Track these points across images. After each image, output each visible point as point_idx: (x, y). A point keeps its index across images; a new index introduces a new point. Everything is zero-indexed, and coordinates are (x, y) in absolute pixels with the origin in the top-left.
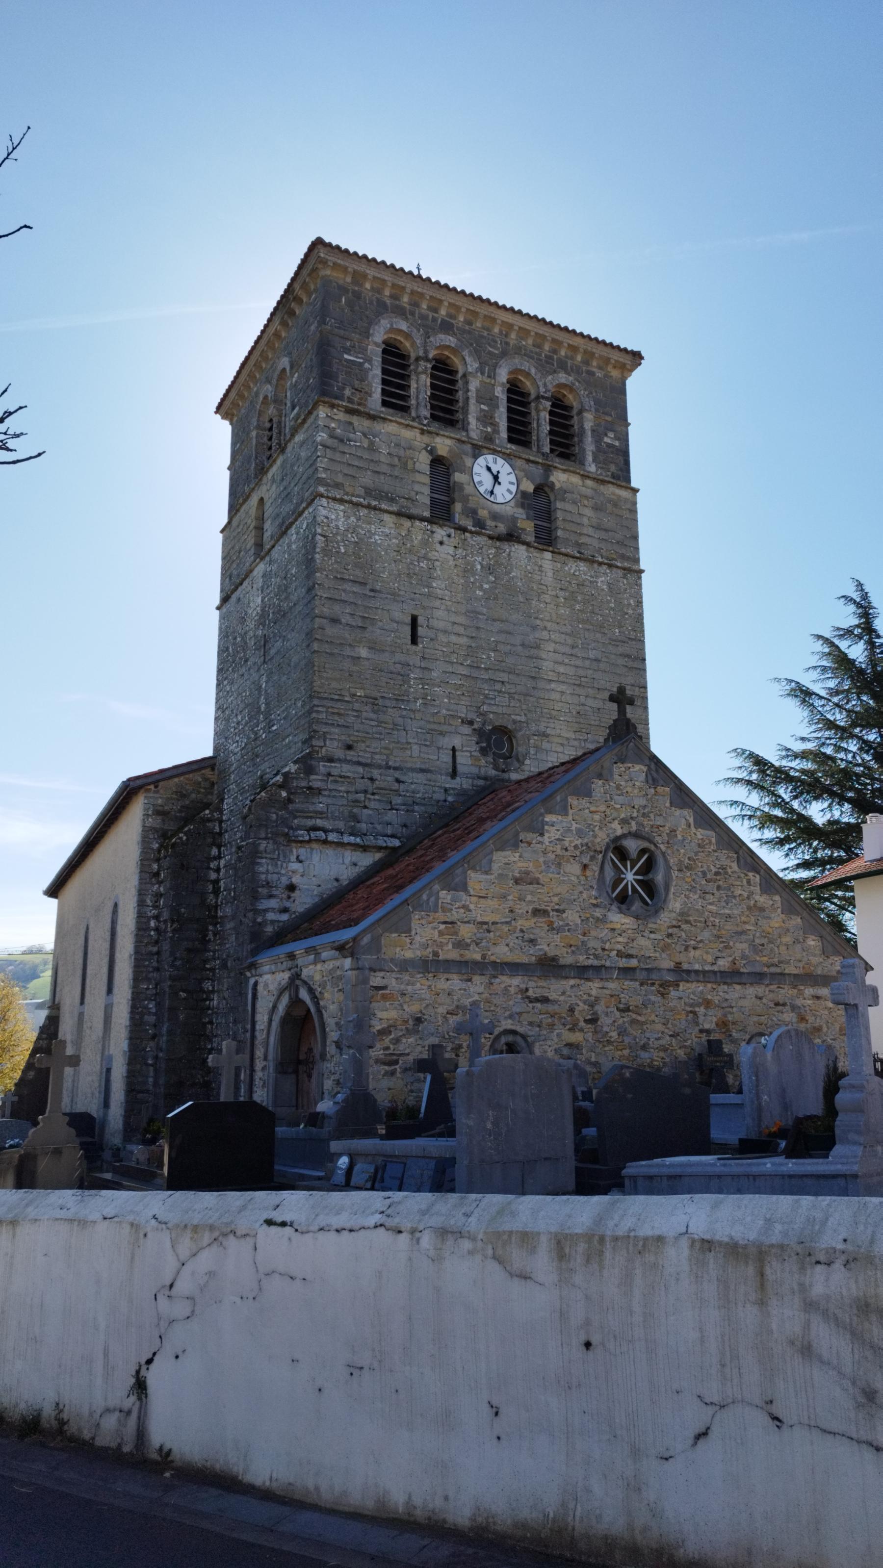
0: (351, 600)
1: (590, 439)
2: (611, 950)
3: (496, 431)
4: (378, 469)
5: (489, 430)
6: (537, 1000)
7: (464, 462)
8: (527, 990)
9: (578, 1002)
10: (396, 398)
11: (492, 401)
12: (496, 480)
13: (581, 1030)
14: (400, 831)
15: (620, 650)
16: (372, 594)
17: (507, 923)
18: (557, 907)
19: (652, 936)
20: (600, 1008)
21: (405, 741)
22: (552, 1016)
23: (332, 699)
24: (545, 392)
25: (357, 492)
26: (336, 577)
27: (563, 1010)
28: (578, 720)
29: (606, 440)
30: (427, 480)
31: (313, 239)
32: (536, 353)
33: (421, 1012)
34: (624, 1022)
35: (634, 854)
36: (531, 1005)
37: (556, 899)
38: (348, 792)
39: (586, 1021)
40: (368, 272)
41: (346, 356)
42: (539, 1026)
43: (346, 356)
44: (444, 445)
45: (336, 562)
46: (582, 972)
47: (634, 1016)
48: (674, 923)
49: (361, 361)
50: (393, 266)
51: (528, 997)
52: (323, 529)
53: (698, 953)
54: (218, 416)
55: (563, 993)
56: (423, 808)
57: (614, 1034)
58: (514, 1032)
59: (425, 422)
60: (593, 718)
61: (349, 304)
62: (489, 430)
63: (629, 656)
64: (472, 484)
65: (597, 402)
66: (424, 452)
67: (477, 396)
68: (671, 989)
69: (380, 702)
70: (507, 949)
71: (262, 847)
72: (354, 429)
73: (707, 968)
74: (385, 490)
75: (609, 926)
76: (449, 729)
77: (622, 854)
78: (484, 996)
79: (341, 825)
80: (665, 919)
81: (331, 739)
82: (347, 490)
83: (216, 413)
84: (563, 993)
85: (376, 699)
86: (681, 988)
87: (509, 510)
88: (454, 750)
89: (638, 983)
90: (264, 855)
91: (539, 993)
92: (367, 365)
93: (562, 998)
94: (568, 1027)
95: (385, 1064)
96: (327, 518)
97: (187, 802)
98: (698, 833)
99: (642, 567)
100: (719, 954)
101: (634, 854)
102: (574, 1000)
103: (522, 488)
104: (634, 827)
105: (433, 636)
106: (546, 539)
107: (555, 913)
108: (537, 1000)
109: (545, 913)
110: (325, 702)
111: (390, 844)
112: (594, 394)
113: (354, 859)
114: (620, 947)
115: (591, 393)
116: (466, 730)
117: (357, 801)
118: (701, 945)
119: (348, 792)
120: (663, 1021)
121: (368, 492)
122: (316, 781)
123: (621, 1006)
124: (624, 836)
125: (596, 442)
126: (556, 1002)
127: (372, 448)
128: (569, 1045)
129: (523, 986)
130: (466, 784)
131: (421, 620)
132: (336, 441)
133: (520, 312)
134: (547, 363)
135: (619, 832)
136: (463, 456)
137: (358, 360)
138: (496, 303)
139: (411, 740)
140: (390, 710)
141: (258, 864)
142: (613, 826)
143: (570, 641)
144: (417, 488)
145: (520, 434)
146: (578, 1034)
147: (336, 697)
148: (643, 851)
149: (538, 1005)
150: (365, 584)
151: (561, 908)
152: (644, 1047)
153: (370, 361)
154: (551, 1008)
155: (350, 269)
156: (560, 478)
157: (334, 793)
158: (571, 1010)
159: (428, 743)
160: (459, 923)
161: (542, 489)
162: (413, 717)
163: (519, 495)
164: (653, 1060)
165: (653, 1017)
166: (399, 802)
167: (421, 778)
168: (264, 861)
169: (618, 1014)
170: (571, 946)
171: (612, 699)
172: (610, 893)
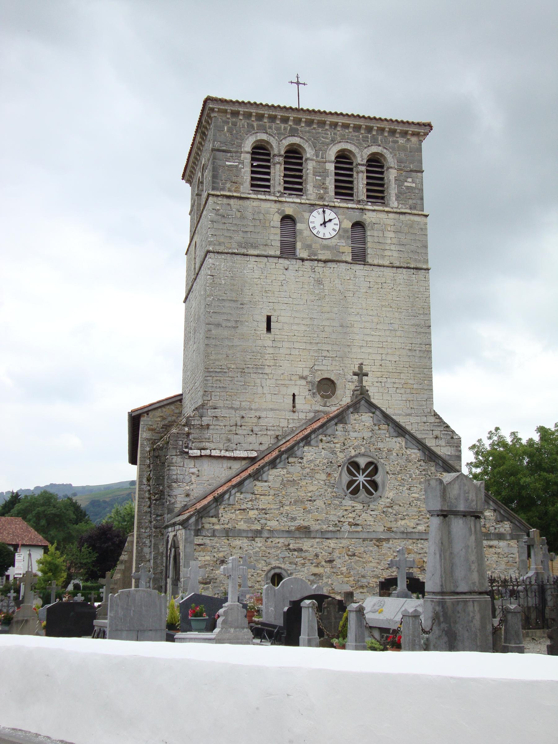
0: (229, 312)
1: (394, 186)
2: (344, 522)
3: (326, 193)
4: (246, 230)
5: (322, 192)
6: (295, 550)
7: (303, 215)
8: (289, 545)
9: (322, 551)
10: (260, 182)
11: (324, 173)
12: (324, 225)
13: (323, 566)
14: (257, 447)
15: (413, 322)
16: (242, 306)
17: (277, 508)
18: (310, 499)
19: (372, 513)
20: (336, 554)
21: (261, 392)
22: (304, 559)
23: (216, 372)
24: (362, 161)
25: (233, 246)
26: (219, 299)
27: (310, 556)
28: (380, 370)
29: (406, 184)
30: (278, 231)
31: (203, 99)
32: (356, 136)
33: (224, 557)
34: (351, 563)
35: (362, 466)
36: (291, 553)
37: (309, 494)
38: (225, 426)
39: (325, 562)
40: (240, 109)
41: (228, 163)
42: (296, 564)
43: (228, 163)
44: (291, 204)
45: (219, 290)
46: (324, 535)
47: (358, 559)
48: (388, 505)
49: (237, 164)
50: (255, 103)
51: (289, 549)
52: (211, 272)
53: (403, 522)
54: (184, 181)
55: (312, 546)
56: (273, 432)
57: (344, 569)
58: (280, 568)
59: (278, 195)
60: (391, 368)
61: (230, 130)
62: (322, 192)
63: (418, 325)
64: (308, 228)
65: (400, 161)
66: (276, 214)
67: (314, 172)
68: (384, 543)
69: (246, 370)
70: (277, 523)
71: (174, 461)
72: (231, 208)
73: (410, 530)
74: (251, 242)
75: (343, 508)
76: (290, 382)
77: (356, 465)
78: (262, 548)
79: (221, 446)
80: (383, 502)
81: (215, 395)
82: (227, 246)
83: (183, 179)
84: (312, 546)
85: (243, 369)
86: (391, 542)
87: (334, 242)
88: (294, 395)
89: (361, 540)
90: (176, 465)
91: (296, 546)
92: (240, 166)
93: (311, 549)
94: (314, 565)
95: (203, 583)
96: (214, 264)
97: (166, 422)
98: (407, 451)
99: (429, 267)
100: (419, 522)
101: (362, 466)
102: (318, 550)
103: (343, 226)
104: (363, 450)
105: (281, 327)
106: (360, 257)
107: (309, 502)
108: (295, 550)
109: (302, 502)
110: (211, 374)
111: (250, 456)
112: (398, 155)
113: (229, 465)
114: (351, 520)
115: (395, 155)
116: (303, 382)
117: (231, 431)
118: (406, 517)
119: (225, 426)
120: (377, 561)
121: (240, 245)
122: (206, 420)
123: (350, 553)
124: (356, 456)
125: (399, 186)
126: (307, 551)
127: (243, 218)
128: (315, 575)
129: (287, 543)
130: (302, 416)
131: (273, 319)
132: (220, 217)
133: (341, 114)
134: (364, 141)
135: (353, 453)
136: (303, 213)
137: (235, 164)
138: (325, 112)
139: (265, 392)
140: (252, 375)
141: (172, 470)
142: (349, 450)
143: (375, 320)
144: (272, 237)
145: (344, 189)
146: (320, 568)
147: (219, 370)
148: (369, 464)
149: (296, 553)
150: (237, 301)
151: (313, 499)
152: (363, 577)
153: (243, 163)
154: (303, 554)
155: (228, 111)
156: (369, 218)
157: (217, 427)
158: (317, 556)
159: (276, 393)
160: (248, 510)
161: (358, 225)
162: (267, 377)
163: (341, 232)
164: (369, 583)
165: (371, 559)
166: (257, 430)
167: (270, 414)
168: (175, 468)
169: (347, 558)
170: (318, 520)
171: (355, 374)
172: (345, 489)
